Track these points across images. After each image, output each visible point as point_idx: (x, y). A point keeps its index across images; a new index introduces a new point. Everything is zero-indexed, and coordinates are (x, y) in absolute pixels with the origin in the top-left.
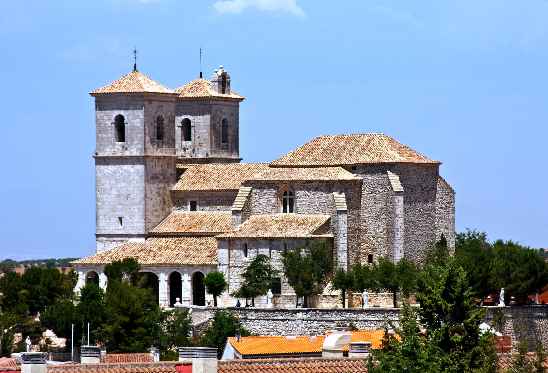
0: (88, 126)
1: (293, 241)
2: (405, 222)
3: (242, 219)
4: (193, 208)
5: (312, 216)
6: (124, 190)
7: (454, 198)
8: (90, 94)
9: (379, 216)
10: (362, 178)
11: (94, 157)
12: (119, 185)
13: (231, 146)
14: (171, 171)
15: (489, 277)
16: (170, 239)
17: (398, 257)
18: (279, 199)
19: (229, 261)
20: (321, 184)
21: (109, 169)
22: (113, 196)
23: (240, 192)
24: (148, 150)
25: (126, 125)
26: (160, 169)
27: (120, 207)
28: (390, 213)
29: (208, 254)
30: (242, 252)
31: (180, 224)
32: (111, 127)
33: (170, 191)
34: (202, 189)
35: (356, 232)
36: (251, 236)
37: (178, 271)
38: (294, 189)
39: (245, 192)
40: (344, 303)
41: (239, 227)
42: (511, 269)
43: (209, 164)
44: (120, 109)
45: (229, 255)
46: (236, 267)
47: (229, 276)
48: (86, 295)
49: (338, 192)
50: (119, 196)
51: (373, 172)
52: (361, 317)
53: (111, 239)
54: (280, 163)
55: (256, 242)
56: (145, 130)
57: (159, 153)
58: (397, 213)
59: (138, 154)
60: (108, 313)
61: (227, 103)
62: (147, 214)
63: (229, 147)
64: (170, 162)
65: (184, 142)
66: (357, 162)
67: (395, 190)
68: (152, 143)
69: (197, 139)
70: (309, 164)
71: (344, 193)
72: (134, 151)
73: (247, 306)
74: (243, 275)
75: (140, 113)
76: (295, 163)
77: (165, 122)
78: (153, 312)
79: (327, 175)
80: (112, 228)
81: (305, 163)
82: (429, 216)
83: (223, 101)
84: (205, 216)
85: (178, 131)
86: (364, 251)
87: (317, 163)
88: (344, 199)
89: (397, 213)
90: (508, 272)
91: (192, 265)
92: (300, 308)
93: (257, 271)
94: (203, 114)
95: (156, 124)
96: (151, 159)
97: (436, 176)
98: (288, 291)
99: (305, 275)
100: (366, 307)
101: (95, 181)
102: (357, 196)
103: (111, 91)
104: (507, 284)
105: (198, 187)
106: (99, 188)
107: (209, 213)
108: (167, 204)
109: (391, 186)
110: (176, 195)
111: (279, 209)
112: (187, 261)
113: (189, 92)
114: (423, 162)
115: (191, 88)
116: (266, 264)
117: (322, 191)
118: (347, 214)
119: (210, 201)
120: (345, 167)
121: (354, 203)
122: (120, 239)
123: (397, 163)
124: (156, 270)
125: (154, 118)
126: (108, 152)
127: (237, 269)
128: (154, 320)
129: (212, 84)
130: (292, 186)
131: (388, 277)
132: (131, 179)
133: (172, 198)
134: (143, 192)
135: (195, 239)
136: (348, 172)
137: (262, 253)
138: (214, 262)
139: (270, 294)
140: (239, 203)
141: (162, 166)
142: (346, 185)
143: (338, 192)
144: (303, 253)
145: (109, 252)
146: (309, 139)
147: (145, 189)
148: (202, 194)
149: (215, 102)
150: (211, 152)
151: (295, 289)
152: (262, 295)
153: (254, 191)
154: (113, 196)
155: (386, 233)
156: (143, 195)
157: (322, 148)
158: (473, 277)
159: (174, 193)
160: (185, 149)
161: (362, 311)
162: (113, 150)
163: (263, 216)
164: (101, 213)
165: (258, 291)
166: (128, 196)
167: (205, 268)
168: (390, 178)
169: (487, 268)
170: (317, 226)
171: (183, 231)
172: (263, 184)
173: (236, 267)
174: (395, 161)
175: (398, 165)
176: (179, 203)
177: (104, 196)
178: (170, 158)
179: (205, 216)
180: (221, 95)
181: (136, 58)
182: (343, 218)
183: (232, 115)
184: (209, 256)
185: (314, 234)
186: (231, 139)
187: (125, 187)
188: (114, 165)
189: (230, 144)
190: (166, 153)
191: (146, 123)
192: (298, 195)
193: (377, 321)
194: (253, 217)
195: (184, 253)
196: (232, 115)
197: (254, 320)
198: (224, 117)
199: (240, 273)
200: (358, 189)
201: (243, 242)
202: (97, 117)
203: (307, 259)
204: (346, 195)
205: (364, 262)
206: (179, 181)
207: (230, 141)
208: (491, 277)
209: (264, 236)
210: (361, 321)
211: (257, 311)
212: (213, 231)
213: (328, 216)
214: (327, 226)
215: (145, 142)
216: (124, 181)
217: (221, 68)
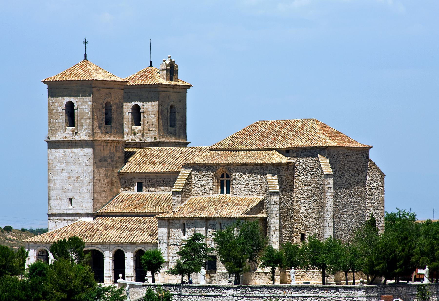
0: (38, 111)
1: (228, 221)
2: (335, 203)
3: (182, 200)
4: (140, 189)
5: (247, 197)
7: (384, 180)
8: (43, 81)
9: (311, 197)
10: (294, 161)
11: (46, 141)
12: (69, 168)
13: (179, 130)
14: (120, 154)
15: (412, 255)
16: (117, 218)
17: (328, 235)
18: (216, 181)
19: (169, 239)
20: (256, 167)
21: (60, 152)
22: (63, 178)
23: (180, 174)
24: (96, 135)
25: (75, 111)
26: (108, 152)
27: (71, 188)
28: (320, 194)
29: (150, 232)
30: (180, 231)
31: (126, 204)
32: (62, 113)
33: (118, 173)
34: (148, 171)
35: (288, 213)
36: (188, 216)
37: (121, 249)
38: (230, 172)
39: (185, 175)
40: (273, 280)
41: (178, 207)
42: (435, 248)
43: (155, 148)
44: (70, 96)
45: (169, 233)
46: (175, 245)
47: (168, 253)
48: (34, 272)
49: (271, 175)
50: (69, 178)
51: (305, 155)
53: (62, 218)
54: (219, 147)
55: (193, 222)
56: (93, 115)
57: (107, 138)
58: (327, 194)
59: (87, 138)
60: (47, 290)
61: (175, 90)
62: (95, 195)
63: (177, 131)
64: (118, 145)
65: (134, 127)
66: (290, 146)
67: (325, 173)
68: (100, 128)
69: (146, 124)
70: (246, 148)
71: (276, 176)
72: (83, 136)
73: (183, 282)
74: (179, 253)
75: (89, 100)
76: (233, 147)
77: (113, 108)
78: (90, 289)
79: (261, 158)
80: (63, 208)
81: (242, 147)
82: (360, 197)
83: (170, 88)
84: (151, 197)
85: (128, 116)
86: (297, 230)
87: (254, 147)
88: (277, 181)
89: (327, 194)
90: (432, 250)
91: (134, 244)
92: (230, 285)
93: (192, 249)
94: (151, 101)
95: (104, 110)
96: (100, 143)
98: (221, 268)
99: (236, 253)
100: (294, 284)
101: (47, 164)
102: (290, 178)
103: (62, 79)
104: (431, 261)
105: (144, 170)
106: (51, 170)
107: (155, 193)
108: (115, 185)
109: (321, 169)
110: (123, 176)
111: (216, 190)
112: (130, 240)
113: (139, 79)
114: (354, 146)
115: (141, 76)
116: (202, 242)
117: (256, 173)
118: (279, 195)
119: (155, 182)
120: (279, 150)
121: (286, 187)
122: (70, 218)
123: (327, 147)
124: (102, 248)
125: (102, 104)
126: (59, 137)
127: (176, 247)
128: (90, 297)
129: (161, 72)
130: (228, 168)
131: (316, 255)
132: (80, 162)
133: (120, 179)
134: (91, 174)
135: (139, 218)
136: (281, 156)
137: (199, 232)
138: (154, 241)
140: (179, 185)
141: (110, 150)
142: (279, 168)
143: (271, 175)
144: (236, 233)
145: (58, 230)
146: (247, 123)
147: (93, 171)
148: (148, 176)
149: (163, 89)
150: (159, 136)
151: (226, 267)
152: (197, 272)
153: (193, 173)
154: (63, 178)
155: (318, 214)
156: (91, 177)
157: (259, 132)
158: (395, 256)
159: (122, 175)
160: (135, 134)
161: (290, 288)
162: (64, 134)
163: (202, 196)
165: (192, 269)
166: (78, 178)
167: (146, 246)
168: (321, 161)
169: (410, 247)
170: (250, 206)
171: (128, 211)
172: (202, 167)
173: (175, 245)
174: (325, 145)
175: (329, 149)
176: (127, 184)
177: (56, 178)
178: (118, 142)
179: (151, 197)
180: (168, 83)
181: (86, 48)
182: (276, 199)
183: (180, 101)
184: (151, 235)
185: (247, 214)
186: (179, 124)
187: (75, 170)
188: (64, 148)
189: (177, 129)
190: (114, 137)
191: (94, 109)
192: (234, 177)
193: (304, 297)
194: (192, 198)
195: (128, 232)
196: (180, 101)
197: (188, 296)
198: (172, 103)
199: (179, 251)
200: (291, 171)
201: (182, 222)
202: (49, 104)
203: (239, 238)
204: (278, 177)
205: (296, 241)
206: (127, 164)
208: (414, 256)
209: (201, 216)
210: (288, 297)
212: (156, 211)
213: (261, 197)
214: (260, 206)
215: (93, 127)
216: (74, 164)
217: (169, 57)
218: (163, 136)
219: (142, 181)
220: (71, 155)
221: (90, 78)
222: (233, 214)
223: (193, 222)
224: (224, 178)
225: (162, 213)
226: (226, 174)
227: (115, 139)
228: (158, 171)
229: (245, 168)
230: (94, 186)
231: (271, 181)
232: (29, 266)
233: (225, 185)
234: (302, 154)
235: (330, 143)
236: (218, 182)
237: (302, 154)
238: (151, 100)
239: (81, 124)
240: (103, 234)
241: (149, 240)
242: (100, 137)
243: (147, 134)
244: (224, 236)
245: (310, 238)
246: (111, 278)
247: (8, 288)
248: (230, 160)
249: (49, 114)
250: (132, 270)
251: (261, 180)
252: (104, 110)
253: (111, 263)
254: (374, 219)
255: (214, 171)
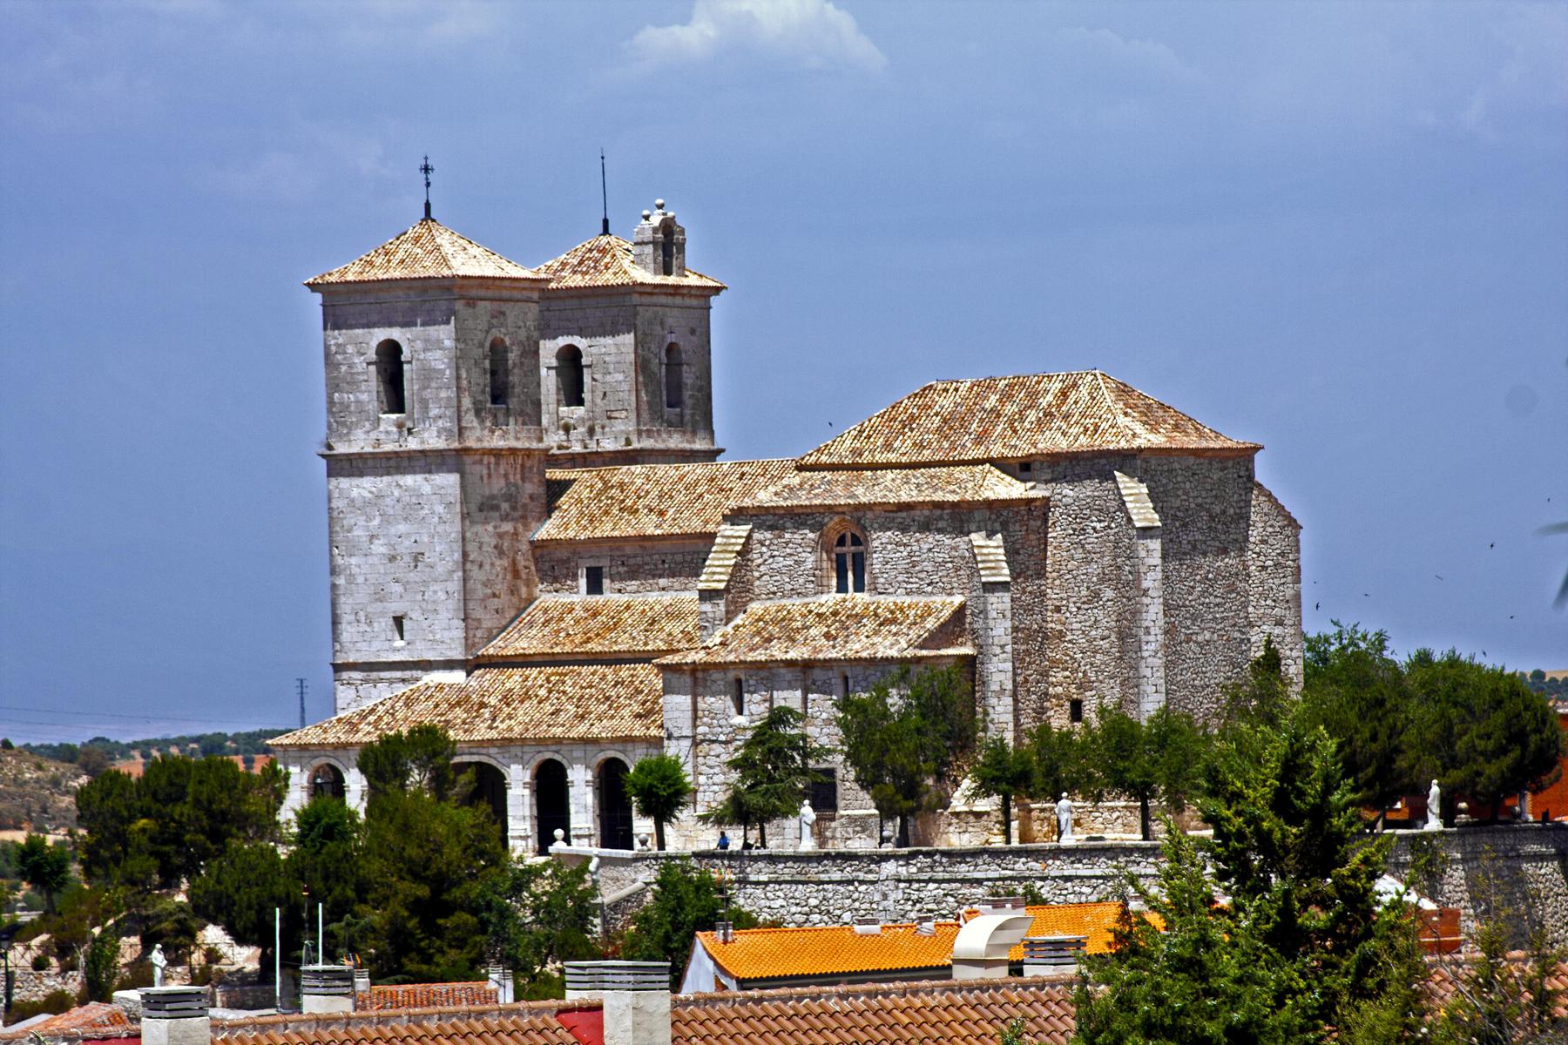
1: (865, 668)
2: (1168, 608)
3: (727, 612)
4: (595, 587)
5: (916, 599)
6: (407, 543)
7: (1298, 541)
9: (1096, 595)
10: (1047, 494)
11: (323, 456)
12: (393, 531)
13: (693, 415)
15: (1397, 750)
16: (535, 671)
17: (1150, 705)
19: (695, 726)
20: (938, 512)
21: (362, 487)
22: (375, 560)
23: (718, 540)
24: (467, 433)
25: (406, 367)
26: (502, 482)
27: (398, 588)
29: (637, 708)
31: (558, 631)
33: (531, 542)
34: (616, 533)
35: (1033, 641)
37: (557, 757)
38: (864, 528)
41: (718, 633)
43: (633, 468)
44: (391, 325)
47: (695, 767)
48: (312, 828)
50: (392, 559)
52: (1056, 868)
53: (374, 675)
55: (768, 674)
56: (458, 378)
57: (497, 442)
58: (1145, 584)
59: (441, 444)
61: (678, 300)
62: (471, 605)
63: (687, 418)
64: (528, 463)
65: (563, 409)
66: (1033, 451)
67: (1138, 525)
68: (478, 413)
69: (599, 401)
70: (904, 459)
71: (999, 536)
72: (431, 438)
74: (734, 765)
75: (445, 334)
76: (866, 458)
77: (513, 356)
78: (493, 870)
80: (376, 645)
81: (892, 457)
84: (628, 608)
85: (549, 381)
86: (1059, 690)
87: (926, 455)
88: (1002, 551)
89: (1145, 584)
90: (1448, 736)
91: (595, 741)
92: (888, 848)
93: (770, 751)
94: (614, 334)
95: (487, 362)
97: (1249, 482)
98: (856, 803)
99: (901, 759)
100: (1068, 840)
103: (365, 277)
105: (605, 530)
106: (339, 538)
107: (639, 598)
108: (524, 576)
109: (1127, 512)
110: (545, 551)
112: (581, 730)
113: (575, 272)
114: (1212, 445)
115: (580, 263)
116: (795, 731)
117: (940, 531)
118: (1008, 590)
119: (640, 566)
120: (1001, 464)
121: (1028, 561)
122: (398, 674)
123: (1140, 450)
124: (499, 757)
125: (481, 345)
126: (358, 443)
127: (717, 748)
130: (859, 520)
134: (457, 547)
135: (601, 669)
136: (1008, 478)
137: (783, 703)
138: (654, 732)
139: (808, 812)
141: (506, 476)
144: (895, 700)
145: (367, 709)
147: (464, 539)
149: (646, 300)
150: (640, 433)
151: (874, 798)
152: (785, 816)
153: (756, 536)
156: (457, 556)
157: (937, 414)
158: (1354, 753)
160: (567, 429)
161: (1057, 853)
162: (373, 435)
163: (784, 602)
164: (346, 606)
166: (417, 558)
167: (629, 747)
169: (1393, 728)
171: (567, 649)
172: (782, 517)
173: (714, 742)
176: (557, 572)
177: (353, 561)
178: (528, 453)
179: (628, 608)
180: (660, 279)
181: (428, 185)
183: (693, 332)
184: (639, 716)
185: (921, 647)
186: (691, 396)
188: (376, 475)
189: (688, 412)
190: (517, 439)
191: (459, 360)
192: (876, 543)
194: (755, 607)
196: (693, 332)
197: (766, 884)
198: (671, 338)
199: (725, 758)
201: (731, 675)
202: (327, 347)
203: (904, 717)
204: (1005, 540)
205: (1059, 721)
207: (689, 402)
208: (1403, 752)
209: (788, 657)
210: (1054, 879)
211: (773, 859)
213: (958, 600)
214: (954, 627)
216: (406, 519)
217: (660, 207)
218: (649, 433)
219: (603, 563)
220: (396, 493)
221: (446, 272)
222: (881, 649)
223: (763, 674)
224: (846, 545)
225: (668, 652)
226: (853, 535)
227: (519, 445)
228: (649, 532)
229: (903, 516)
230: (465, 580)
231: (985, 551)
232: (296, 813)
233: (850, 567)
234: (1069, 472)
235: (1147, 439)
236: (829, 559)
237: (1069, 472)
238: (612, 329)
239: (425, 408)
240: (503, 716)
241: (638, 731)
242: (483, 437)
243: (603, 427)
244: (865, 711)
245: (1102, 712)
246: (530, 841)
247: (252, 876)
248: (863, 495)
249: (328, 379)
250: (590, 816)
251: (955, 549)
252: (487, 363)
253: (527, 800)
254: (1276, 651)
255: (817, 527)
